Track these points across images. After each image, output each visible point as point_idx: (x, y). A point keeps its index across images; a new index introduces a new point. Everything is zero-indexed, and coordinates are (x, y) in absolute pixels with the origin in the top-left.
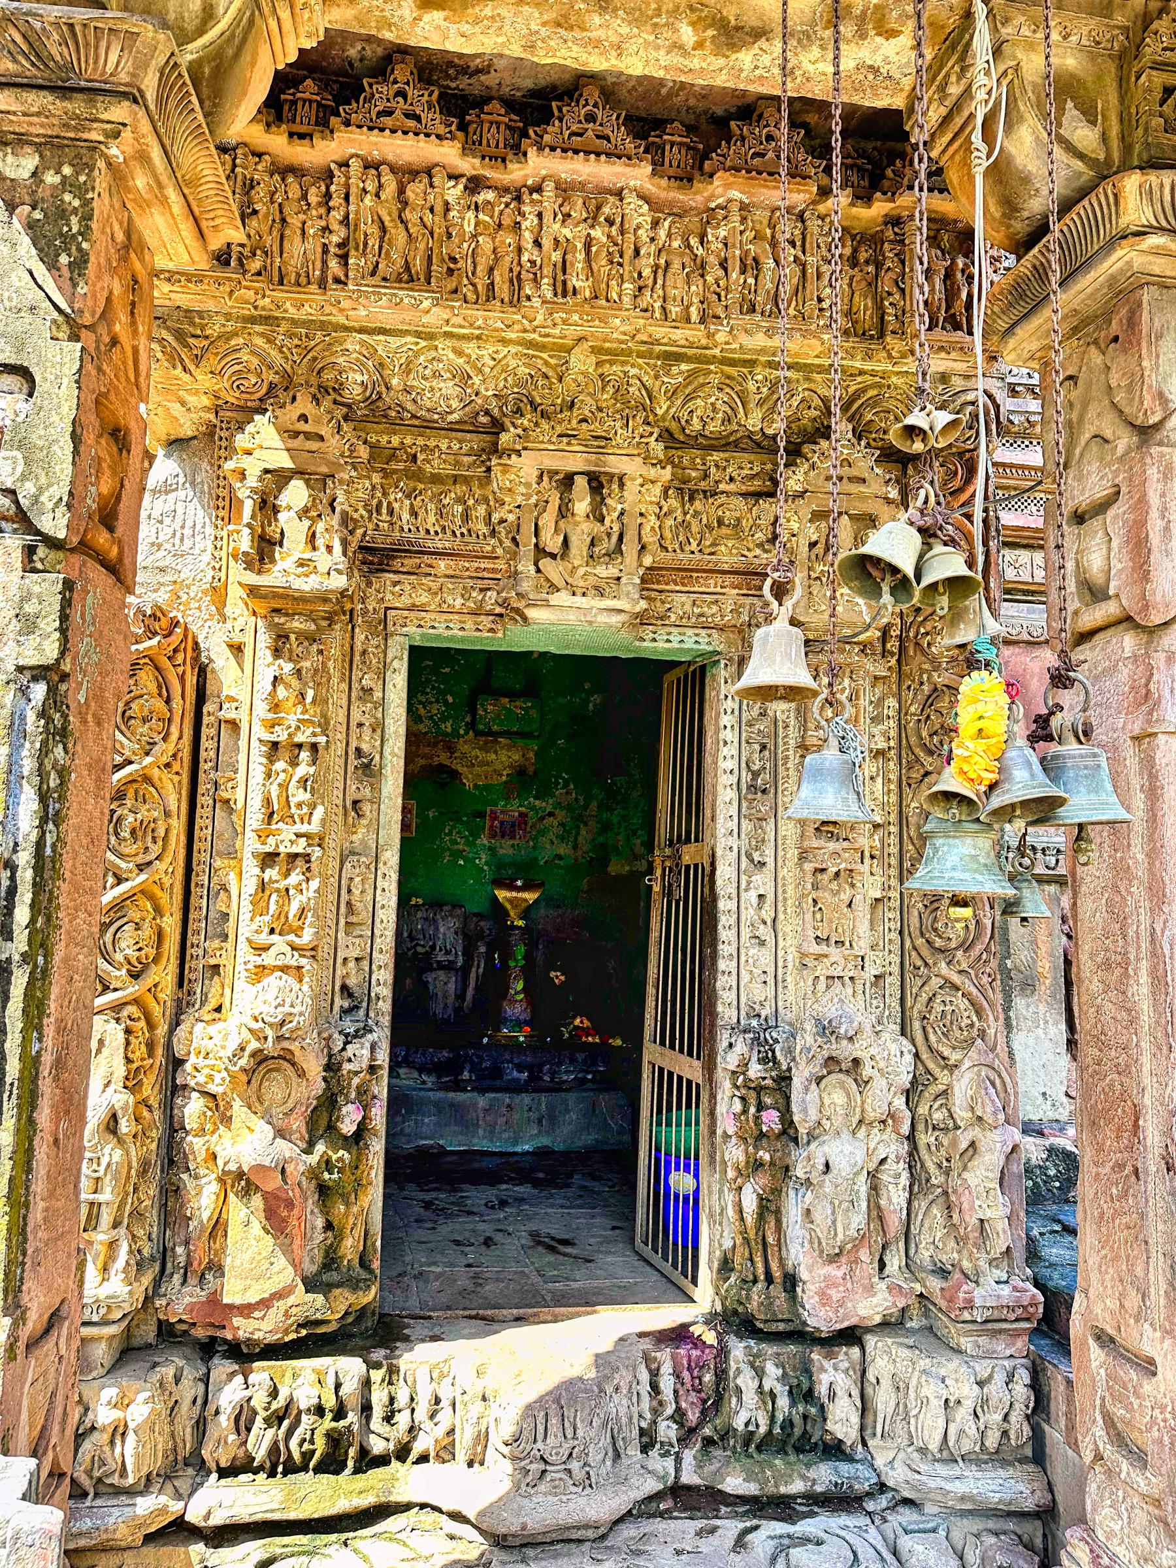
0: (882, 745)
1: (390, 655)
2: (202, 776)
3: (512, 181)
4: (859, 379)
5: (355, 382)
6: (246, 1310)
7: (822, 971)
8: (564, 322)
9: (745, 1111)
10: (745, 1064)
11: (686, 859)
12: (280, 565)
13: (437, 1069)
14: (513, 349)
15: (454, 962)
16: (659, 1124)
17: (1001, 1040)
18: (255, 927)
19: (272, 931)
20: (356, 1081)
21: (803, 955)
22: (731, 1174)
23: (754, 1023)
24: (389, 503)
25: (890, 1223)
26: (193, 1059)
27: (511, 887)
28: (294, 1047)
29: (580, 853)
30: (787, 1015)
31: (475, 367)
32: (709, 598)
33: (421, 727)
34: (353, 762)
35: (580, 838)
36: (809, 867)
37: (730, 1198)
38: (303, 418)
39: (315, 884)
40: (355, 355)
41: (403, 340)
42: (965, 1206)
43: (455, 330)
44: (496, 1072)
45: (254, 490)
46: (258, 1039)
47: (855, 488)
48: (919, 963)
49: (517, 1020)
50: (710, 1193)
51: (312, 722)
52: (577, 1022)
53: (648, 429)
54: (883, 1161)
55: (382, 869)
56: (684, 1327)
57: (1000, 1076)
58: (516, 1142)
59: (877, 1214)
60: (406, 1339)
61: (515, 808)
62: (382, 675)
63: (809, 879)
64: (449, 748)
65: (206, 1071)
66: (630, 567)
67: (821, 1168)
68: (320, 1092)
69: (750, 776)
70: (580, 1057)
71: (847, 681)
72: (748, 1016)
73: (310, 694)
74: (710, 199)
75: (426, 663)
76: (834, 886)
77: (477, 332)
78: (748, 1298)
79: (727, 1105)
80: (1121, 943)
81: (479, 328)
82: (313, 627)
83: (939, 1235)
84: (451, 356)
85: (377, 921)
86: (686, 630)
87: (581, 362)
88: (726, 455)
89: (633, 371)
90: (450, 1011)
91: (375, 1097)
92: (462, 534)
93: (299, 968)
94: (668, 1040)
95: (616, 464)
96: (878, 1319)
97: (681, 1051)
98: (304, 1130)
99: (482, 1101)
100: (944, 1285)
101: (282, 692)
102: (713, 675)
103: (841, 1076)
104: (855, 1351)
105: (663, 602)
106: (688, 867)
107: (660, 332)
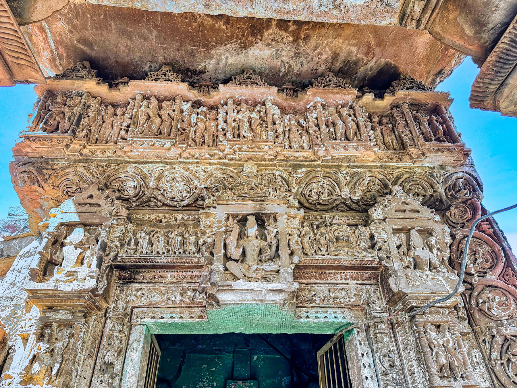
1: (132, 339)
3: (214, 102)
4: (398, 170)
5: (130, 188)
8: (240, 149)
12: (56, 276)
14: (215, 167)
24: (136, 239)
31: (194, 175)
41: (157, 166)
43: (185, 160)
45: (50, 234)
47: (414, 215)
53: (288, 194)
62: (122, 352)
66: (285, 265)
73: (57, 366)
74: (306, 104)
77: (196, 161)
81: (197, 158)
82: (71, 317)
84: (182, 171)
86: (327, 309)
87: (250, 168)
88: (333, 214)
89: (277, 173)
92: (180, 253)
95: (270, 208)
101: (36, 367)
102: (350, 342)
105: (310, 291)
107: (289, 154)
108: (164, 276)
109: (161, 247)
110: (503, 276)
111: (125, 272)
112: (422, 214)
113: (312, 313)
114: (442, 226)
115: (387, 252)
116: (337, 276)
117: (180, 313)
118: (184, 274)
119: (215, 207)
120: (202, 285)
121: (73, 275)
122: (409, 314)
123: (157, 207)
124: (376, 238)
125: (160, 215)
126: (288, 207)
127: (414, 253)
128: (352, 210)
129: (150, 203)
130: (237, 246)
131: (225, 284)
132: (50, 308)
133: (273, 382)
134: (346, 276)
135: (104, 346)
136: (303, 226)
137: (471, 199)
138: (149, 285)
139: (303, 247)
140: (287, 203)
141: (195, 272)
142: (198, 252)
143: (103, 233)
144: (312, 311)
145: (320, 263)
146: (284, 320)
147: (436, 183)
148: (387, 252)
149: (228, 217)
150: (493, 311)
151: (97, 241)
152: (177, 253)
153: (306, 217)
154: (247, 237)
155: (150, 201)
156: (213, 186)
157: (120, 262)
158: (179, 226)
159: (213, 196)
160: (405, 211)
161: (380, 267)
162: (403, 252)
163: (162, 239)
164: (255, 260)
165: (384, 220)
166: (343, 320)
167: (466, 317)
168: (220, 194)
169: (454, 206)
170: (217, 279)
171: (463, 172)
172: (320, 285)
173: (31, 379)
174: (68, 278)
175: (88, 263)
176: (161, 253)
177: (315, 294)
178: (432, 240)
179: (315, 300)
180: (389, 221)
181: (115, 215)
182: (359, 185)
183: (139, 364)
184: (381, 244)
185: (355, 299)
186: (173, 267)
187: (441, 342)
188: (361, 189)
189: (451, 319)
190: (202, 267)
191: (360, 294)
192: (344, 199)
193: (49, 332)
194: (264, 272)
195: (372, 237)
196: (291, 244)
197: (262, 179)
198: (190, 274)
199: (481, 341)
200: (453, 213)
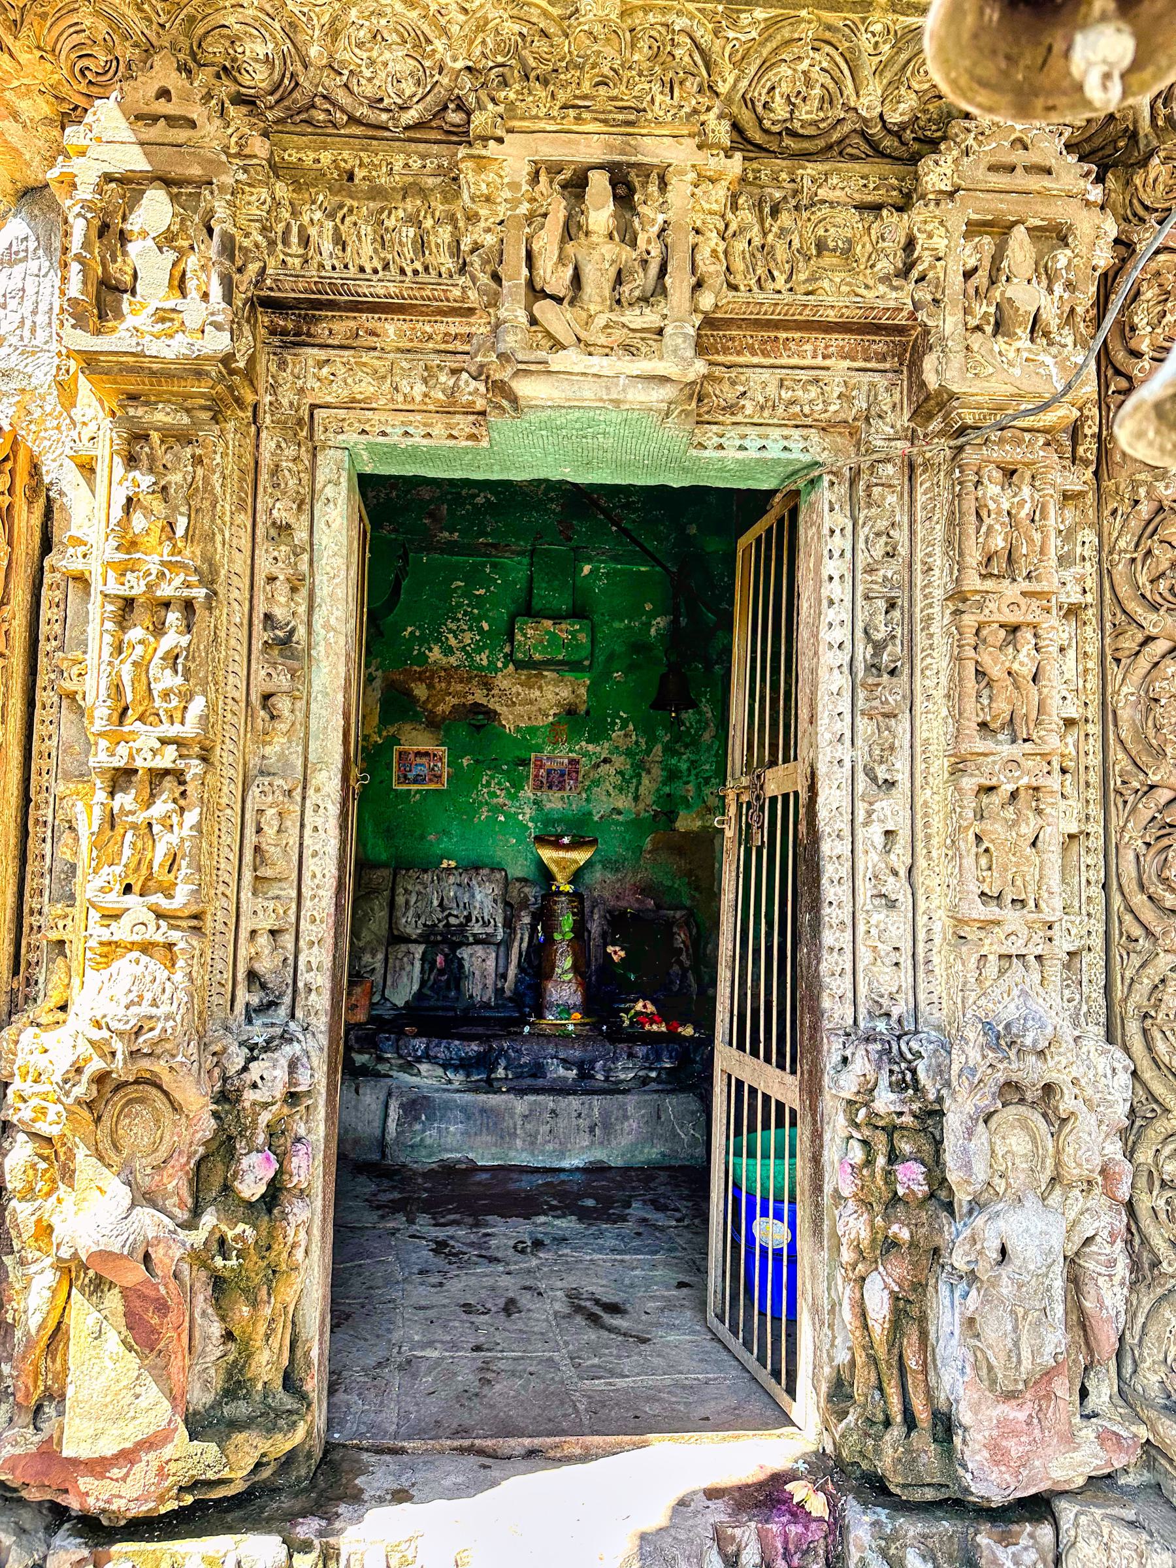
0: (1076, 598)
1: (321, 478)
2: (42, 661)
6: (98, 1467)
7: (993, 946)
9: (869, 1162)
11: (771, 789)
12: (130, 321)
13: (465, 1065)
15: (493, 935)
16: (738, 1154)
18: (99, 882)
19: (128, 889)
20: (265, 1117)
22: (847, 1256)
23: (881, 1026)
24: (302, 228)
25: (1102, 1337)
26: (17, 1085)
27: (557, 845)
28: (159, 1067)
29: (641, 806)
31: (435, 24)
32: (804, 375)
33: (453, 660)
34: (261, 636)
35: (642, 790)
36: (969, 783)
37: (847, 1293)
38: (164, 93)
39: (192, 817)
40: (251, 12)
44: (538, 1070)
45: (87, 205)
46: (103, 1056)
47: (1035, 182)
48: (1137, 931)
49: (566, 1005)
51: (185, 566)
52: (639, 1006)
53: (705, 101)
54: (1089, 1241)
55: (312, 797)
56: (779, 1480)
58: (562, 1155)
59: (1081, 1323)
60: (356, 1497)
61: (560, 755)
62: (306, 503)
63: (970, 803)
64: (485, 684)
65: (34, 1102)
66: (678, 313)
67: (995, 1256)
68: (209, 1135)
69: (870, 650)
71: (1026, 491)
73: (181, 523)
75: (392, 506)
76: (1010, 813)
78: (878, 1451)
79: (841, 1150)
82: (186, 420)
85: (306, 875)
86: (769, 430)
88: (827, 166)
89: (680, 23)
90: (490, 994)
91: (299, 1140)
92: (416, 272)
93: (170, 946)
95: (657, 148)
96: (1081, 1481)
98: (185, 1192)
99: (521, 1105)
101: (139, 521)
102: (811, 505)
104: (1045, 1532)
106: (773, 800)
108: (379, 331)
109: (365, 252)
111: (289, 316)
113: (732, 438)
115: (937, 287)
117: (425, 425)
118: (428, 329)
119: (500, 140)
120: (478, 359)
121: (172, 320)
122: (952, 443)
123: (335, 126)
124: (918, 248)
125: (346, 154)
126: (700, 147)
127: (1003, 293)
128: (882, 155)
129: (314, 112)
130: (560, 258)
131: (532, 358)
132: (133, 397)
133: (628, 628)
134: (826, 347)
135: (265, 488)
136: (735, 207)
138: (346, 353)
139: (728, 269)
140: (699, 134)
141: (456, 325)
142: (462, 270)
143: (221, 211)
148: (937, 287)
149: (537, 172)
151: (210, 231)
152: (409, 273)
153: (750, 176)
154: (587, 234)
155: (313, 106)
156: (491, 64)
157: (271, 289)
158: (405, 192)
159: (493, 100)
160: (1013, 169)
161: (913, 327)
162: (977, 288)
163: (366, 229)
164: (604, 301)
165: (951, 194)
167: (1093, 458)
168: (512, 96)
169: (1162, 154)
170: (513, 344)
173: (133, 544)
174: (160, 326)
175: (198, 288)
176: (368, 270)
179: (743, 407)
181: (238, 155)
182: (912, 73)
183: (344, 532)
184: (926, 265)
185: (837, 407)
186: (400, 309)
187: (1006, 506)
188: (916, 87)
190: (471, 311)
192: (865, 121)
193: (147, 449)
194: (625, 330)
195: (910, 245)
196: (698, 257)
197: (633, 45)
198: (443, 328)
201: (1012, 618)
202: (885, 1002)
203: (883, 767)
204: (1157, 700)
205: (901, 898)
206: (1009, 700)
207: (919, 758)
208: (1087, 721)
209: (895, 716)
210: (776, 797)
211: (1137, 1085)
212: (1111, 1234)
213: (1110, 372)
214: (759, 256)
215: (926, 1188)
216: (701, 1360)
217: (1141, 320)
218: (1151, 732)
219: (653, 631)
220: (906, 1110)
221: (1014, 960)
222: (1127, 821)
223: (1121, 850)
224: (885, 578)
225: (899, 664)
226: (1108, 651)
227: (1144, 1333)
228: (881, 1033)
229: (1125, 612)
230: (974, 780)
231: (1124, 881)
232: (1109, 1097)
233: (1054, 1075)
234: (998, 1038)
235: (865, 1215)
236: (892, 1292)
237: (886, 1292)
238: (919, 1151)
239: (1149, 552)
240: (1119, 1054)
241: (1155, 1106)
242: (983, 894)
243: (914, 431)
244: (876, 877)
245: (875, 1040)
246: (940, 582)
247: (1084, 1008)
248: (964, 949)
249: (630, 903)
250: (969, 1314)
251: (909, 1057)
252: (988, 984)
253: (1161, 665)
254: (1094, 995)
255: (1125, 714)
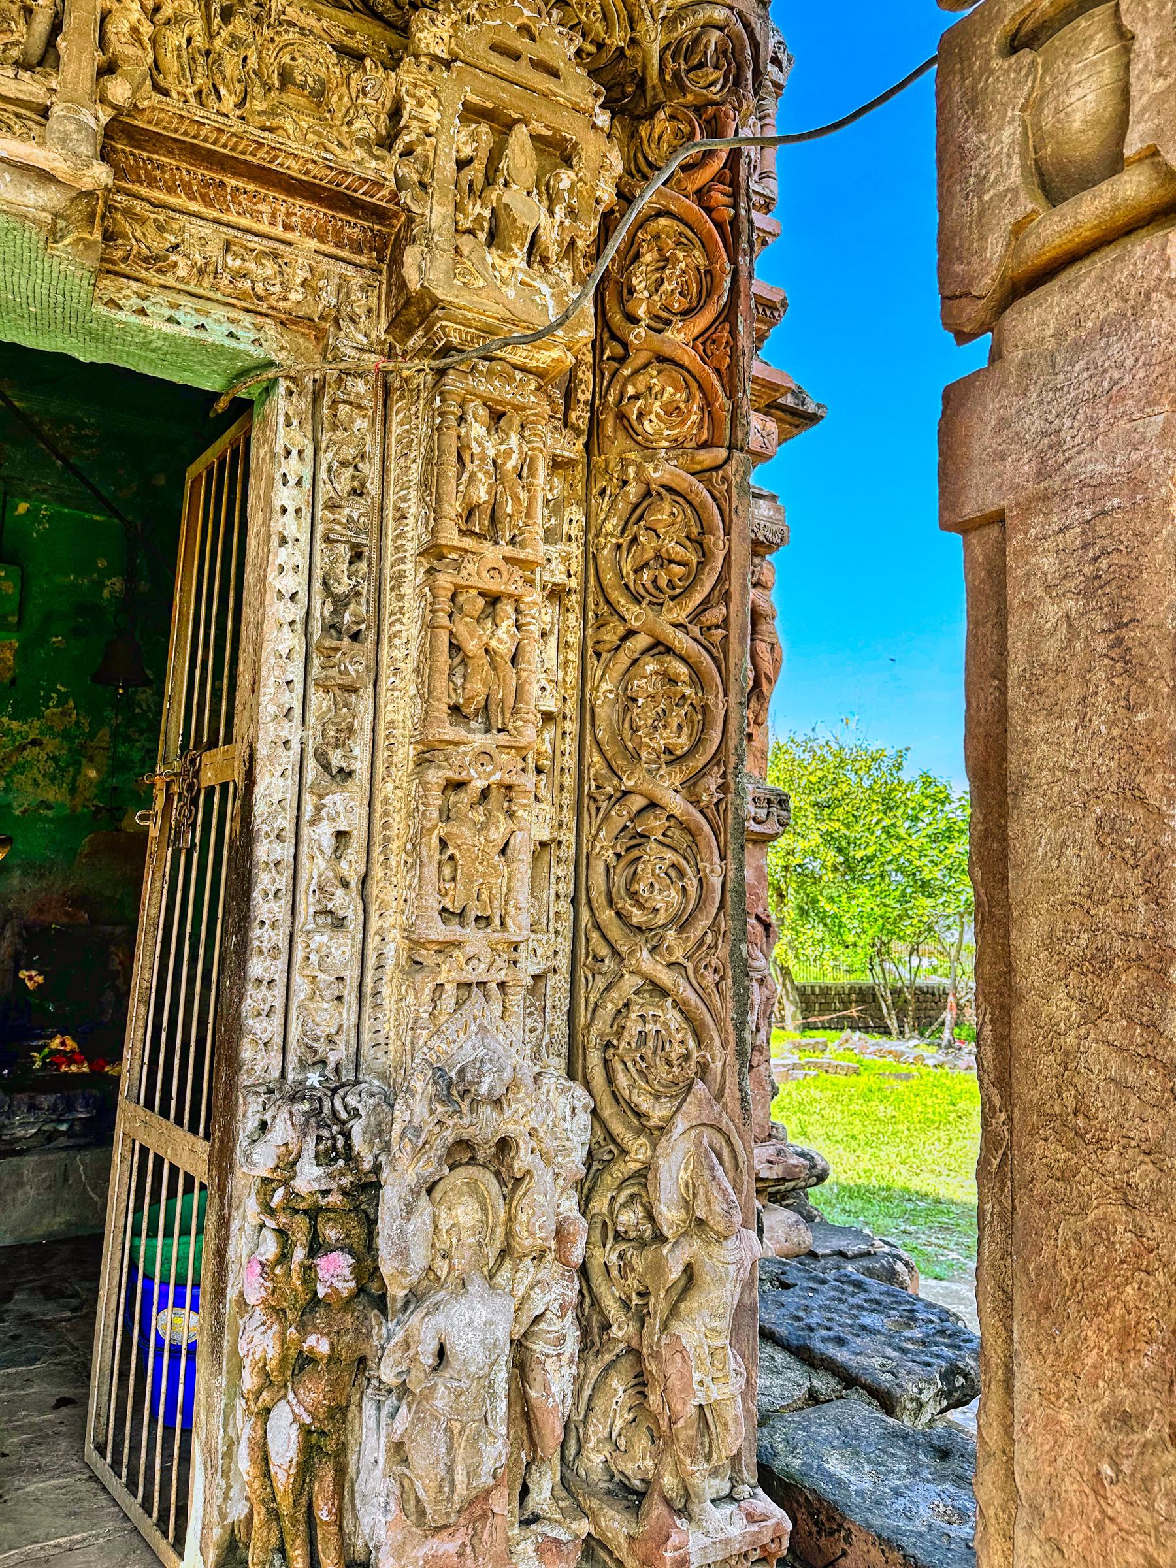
0: (560, 578)
7: (449, 975)
9: (284, 1257)
10: (289, 1164)
11: (208, 777)
17: (731, 1079)
21: (416, 944)
22: (249, 1381)
23: (313, 1078)
25: (547, 1431)
29: (79, 800)
30: (377, 1059)
32: (257, 244)
36: (436, 777)
37: (245, 1430)
42: (675, 1382)
48: (604, 951)
50: (209, 1407)
52: (56, 1043)
54: (538, 1319)
57: (729, 1141)
59: (525, 1415)
67: (430, 1360)
70: (46, 1101)
72: (303, 1065)
76: (479, 815)
79: (251, 1241)
80: (1143, 913)
83: (619, 1424)
86: (210, 306)
94: (157, 1101)
97: (179, 1121)
100: (634, 1529)
102: (265, 417)
103: (472, 1170)
105: (161, 229)
106: (210, 791)
110: (703, 344)
112: (564, 86)
113: (159, 306)
114: (604, 145)
116: (260, 207)
122: (434, 363)
124: (406, 114)
127: (499, 197)
133: (73, 584)
134: (289, 214)
137: (718, 104)
139: (155, 61)
144: (159, 299)
145: (205, 140)
146: (60, 299)
147: (647, 13)
148: (425, 166)
150: (646, 424)
161: (396, 215)
162: (471, 182)
166: (252, 349)
171: (732, 8)
172: (200, 222)
177: (178, 246)
178: (563, 176)
179: (175, 265)
180: (460, 70)
184: (413, 137)
185: (300, 297)
187: (491, 453)
189: (529, 394)
191: (321, 284)
195: (396, 113)
196: (110, 29)
199: (595, 491)
200: (657, 131)
201: (495, 585)
202: (320, 1046)
203: (339, 752)
204: (634, 700)
205: (351, 916)
206: (485, 683)
207: (382, 744)
208: (564, 717)
209: (356, 691)
210: (213, 787)
211: (596, 1124)
212: (562, 1307)
213: (606, 336)
214: (200, 60)
215: (353, 1284)
216: (69, 1515)
217: (640, 283)
218: (627, 734)
219: (106, 593)
220: (334, 1186)
221: (475, 989)
222: (599, 829)
223: (592, 862)
224: (350, 518)
225: (363, 626)
226: (590, 644)
227: (589, 1409)
228: (313, 1088)
229: (608, 602)
230: (441, 773)
231: (593, 895)
232: (568, 1144)
233: (511, 1127)
234: (449, 1087)
235: (276, 1327)
236: (302, 1426)
237: (295, 1426)
238: (347, 1237)
239: (634, 540)
240: (579, 1091)
241: (612, 1147)
242: (444, 910)
243: (392, 347)
244: (321, 889)
245: (303, 1098)
246: (414, 534)
247: (546, 1039)
248: (418, 977)
249: (56, 919)
250: (395, 1438)
251: (344, 1116)
252: (442, 1019)
253: (641, 662)
254: (557, 1023)
255: (602, 712)
